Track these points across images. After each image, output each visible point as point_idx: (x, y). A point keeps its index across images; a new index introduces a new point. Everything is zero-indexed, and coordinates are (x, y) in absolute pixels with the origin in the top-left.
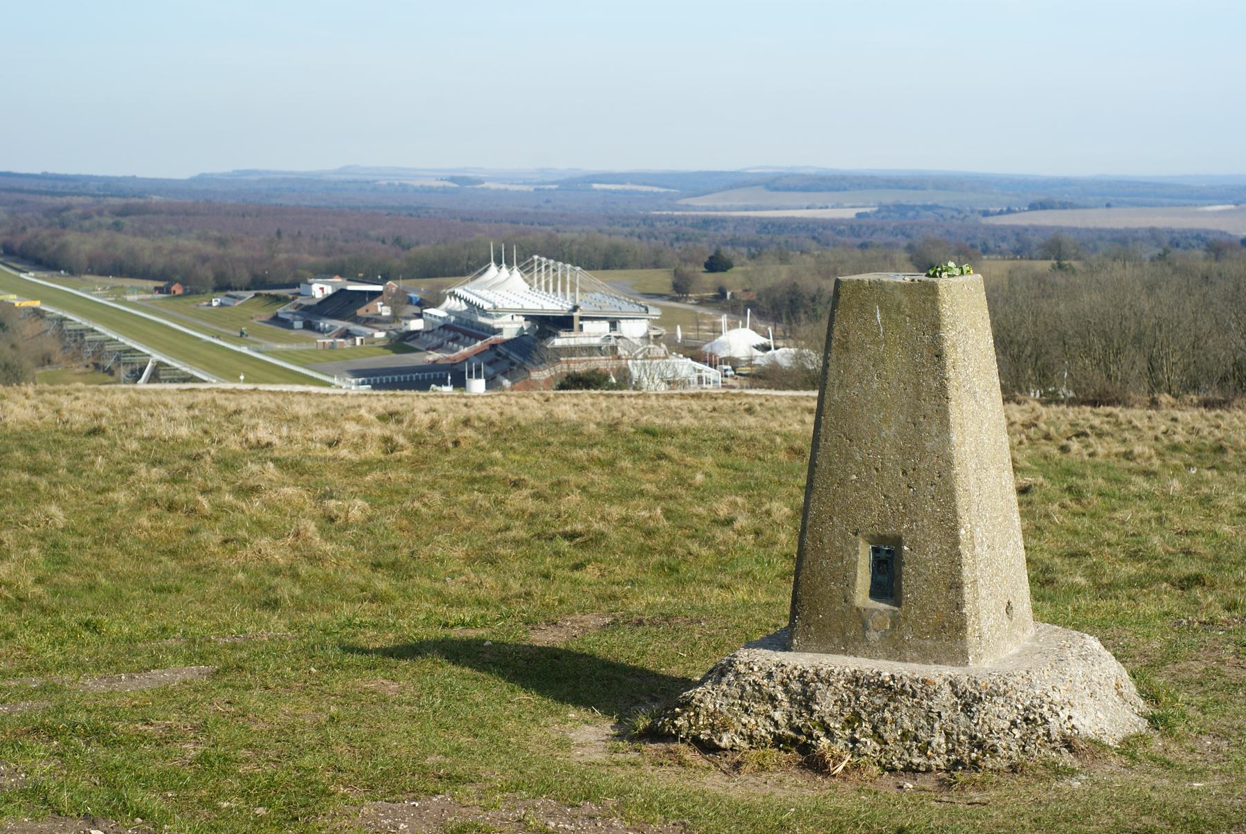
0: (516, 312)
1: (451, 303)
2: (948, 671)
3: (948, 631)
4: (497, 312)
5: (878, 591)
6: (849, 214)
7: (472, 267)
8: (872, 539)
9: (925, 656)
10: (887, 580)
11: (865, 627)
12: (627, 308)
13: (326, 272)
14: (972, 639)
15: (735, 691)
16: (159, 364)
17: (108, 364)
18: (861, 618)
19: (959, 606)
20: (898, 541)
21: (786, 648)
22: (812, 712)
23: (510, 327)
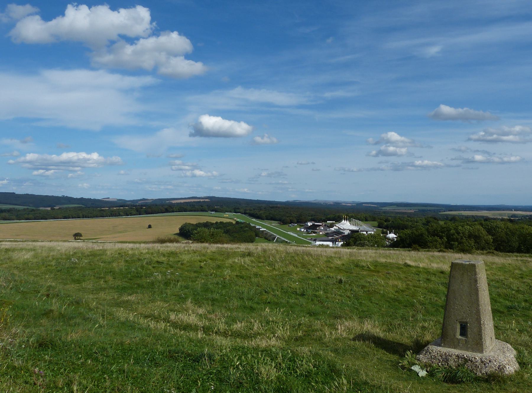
0: (347, 230)
1: (335, 227)
2: (480, 355)
3: (479, 346)
4: (344, 229)
5: (461, 334)
6: (413, 211)
7: (339, 220)
8: (460, 322)
9: (473, 350)
10: (464, 332)
11: (459, 343)
12: (370, 229)
13: (311, 220)
14: (484, 347)
15: (429, 357)
16: (278, 238)
17: (269, 238)
18: (459, 340)
19: (481, 339)
20: (467, 323)
21: (440, 346)
22: (448, 364)
23: (347, 233)
